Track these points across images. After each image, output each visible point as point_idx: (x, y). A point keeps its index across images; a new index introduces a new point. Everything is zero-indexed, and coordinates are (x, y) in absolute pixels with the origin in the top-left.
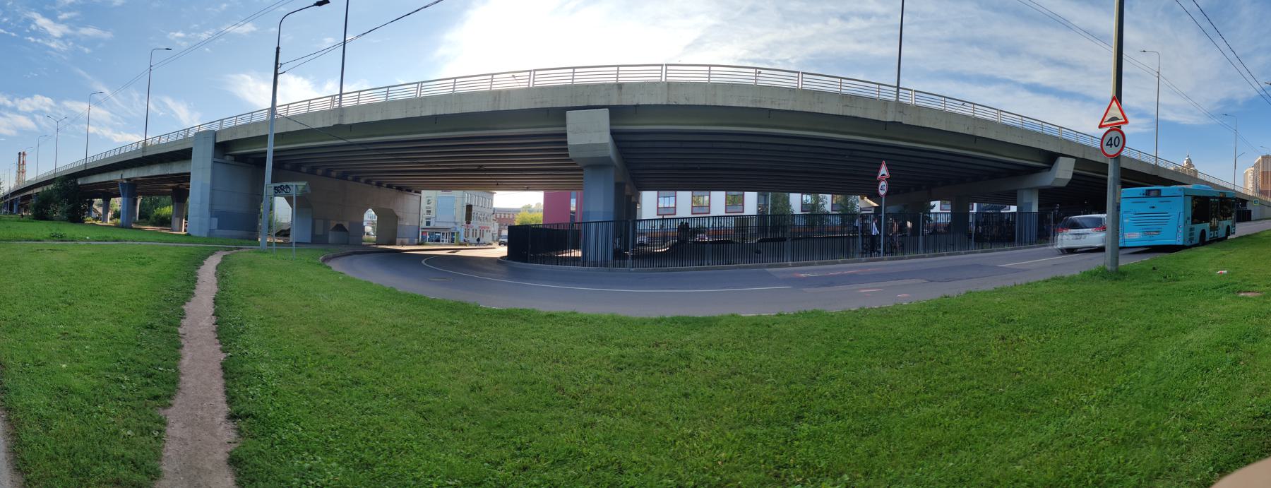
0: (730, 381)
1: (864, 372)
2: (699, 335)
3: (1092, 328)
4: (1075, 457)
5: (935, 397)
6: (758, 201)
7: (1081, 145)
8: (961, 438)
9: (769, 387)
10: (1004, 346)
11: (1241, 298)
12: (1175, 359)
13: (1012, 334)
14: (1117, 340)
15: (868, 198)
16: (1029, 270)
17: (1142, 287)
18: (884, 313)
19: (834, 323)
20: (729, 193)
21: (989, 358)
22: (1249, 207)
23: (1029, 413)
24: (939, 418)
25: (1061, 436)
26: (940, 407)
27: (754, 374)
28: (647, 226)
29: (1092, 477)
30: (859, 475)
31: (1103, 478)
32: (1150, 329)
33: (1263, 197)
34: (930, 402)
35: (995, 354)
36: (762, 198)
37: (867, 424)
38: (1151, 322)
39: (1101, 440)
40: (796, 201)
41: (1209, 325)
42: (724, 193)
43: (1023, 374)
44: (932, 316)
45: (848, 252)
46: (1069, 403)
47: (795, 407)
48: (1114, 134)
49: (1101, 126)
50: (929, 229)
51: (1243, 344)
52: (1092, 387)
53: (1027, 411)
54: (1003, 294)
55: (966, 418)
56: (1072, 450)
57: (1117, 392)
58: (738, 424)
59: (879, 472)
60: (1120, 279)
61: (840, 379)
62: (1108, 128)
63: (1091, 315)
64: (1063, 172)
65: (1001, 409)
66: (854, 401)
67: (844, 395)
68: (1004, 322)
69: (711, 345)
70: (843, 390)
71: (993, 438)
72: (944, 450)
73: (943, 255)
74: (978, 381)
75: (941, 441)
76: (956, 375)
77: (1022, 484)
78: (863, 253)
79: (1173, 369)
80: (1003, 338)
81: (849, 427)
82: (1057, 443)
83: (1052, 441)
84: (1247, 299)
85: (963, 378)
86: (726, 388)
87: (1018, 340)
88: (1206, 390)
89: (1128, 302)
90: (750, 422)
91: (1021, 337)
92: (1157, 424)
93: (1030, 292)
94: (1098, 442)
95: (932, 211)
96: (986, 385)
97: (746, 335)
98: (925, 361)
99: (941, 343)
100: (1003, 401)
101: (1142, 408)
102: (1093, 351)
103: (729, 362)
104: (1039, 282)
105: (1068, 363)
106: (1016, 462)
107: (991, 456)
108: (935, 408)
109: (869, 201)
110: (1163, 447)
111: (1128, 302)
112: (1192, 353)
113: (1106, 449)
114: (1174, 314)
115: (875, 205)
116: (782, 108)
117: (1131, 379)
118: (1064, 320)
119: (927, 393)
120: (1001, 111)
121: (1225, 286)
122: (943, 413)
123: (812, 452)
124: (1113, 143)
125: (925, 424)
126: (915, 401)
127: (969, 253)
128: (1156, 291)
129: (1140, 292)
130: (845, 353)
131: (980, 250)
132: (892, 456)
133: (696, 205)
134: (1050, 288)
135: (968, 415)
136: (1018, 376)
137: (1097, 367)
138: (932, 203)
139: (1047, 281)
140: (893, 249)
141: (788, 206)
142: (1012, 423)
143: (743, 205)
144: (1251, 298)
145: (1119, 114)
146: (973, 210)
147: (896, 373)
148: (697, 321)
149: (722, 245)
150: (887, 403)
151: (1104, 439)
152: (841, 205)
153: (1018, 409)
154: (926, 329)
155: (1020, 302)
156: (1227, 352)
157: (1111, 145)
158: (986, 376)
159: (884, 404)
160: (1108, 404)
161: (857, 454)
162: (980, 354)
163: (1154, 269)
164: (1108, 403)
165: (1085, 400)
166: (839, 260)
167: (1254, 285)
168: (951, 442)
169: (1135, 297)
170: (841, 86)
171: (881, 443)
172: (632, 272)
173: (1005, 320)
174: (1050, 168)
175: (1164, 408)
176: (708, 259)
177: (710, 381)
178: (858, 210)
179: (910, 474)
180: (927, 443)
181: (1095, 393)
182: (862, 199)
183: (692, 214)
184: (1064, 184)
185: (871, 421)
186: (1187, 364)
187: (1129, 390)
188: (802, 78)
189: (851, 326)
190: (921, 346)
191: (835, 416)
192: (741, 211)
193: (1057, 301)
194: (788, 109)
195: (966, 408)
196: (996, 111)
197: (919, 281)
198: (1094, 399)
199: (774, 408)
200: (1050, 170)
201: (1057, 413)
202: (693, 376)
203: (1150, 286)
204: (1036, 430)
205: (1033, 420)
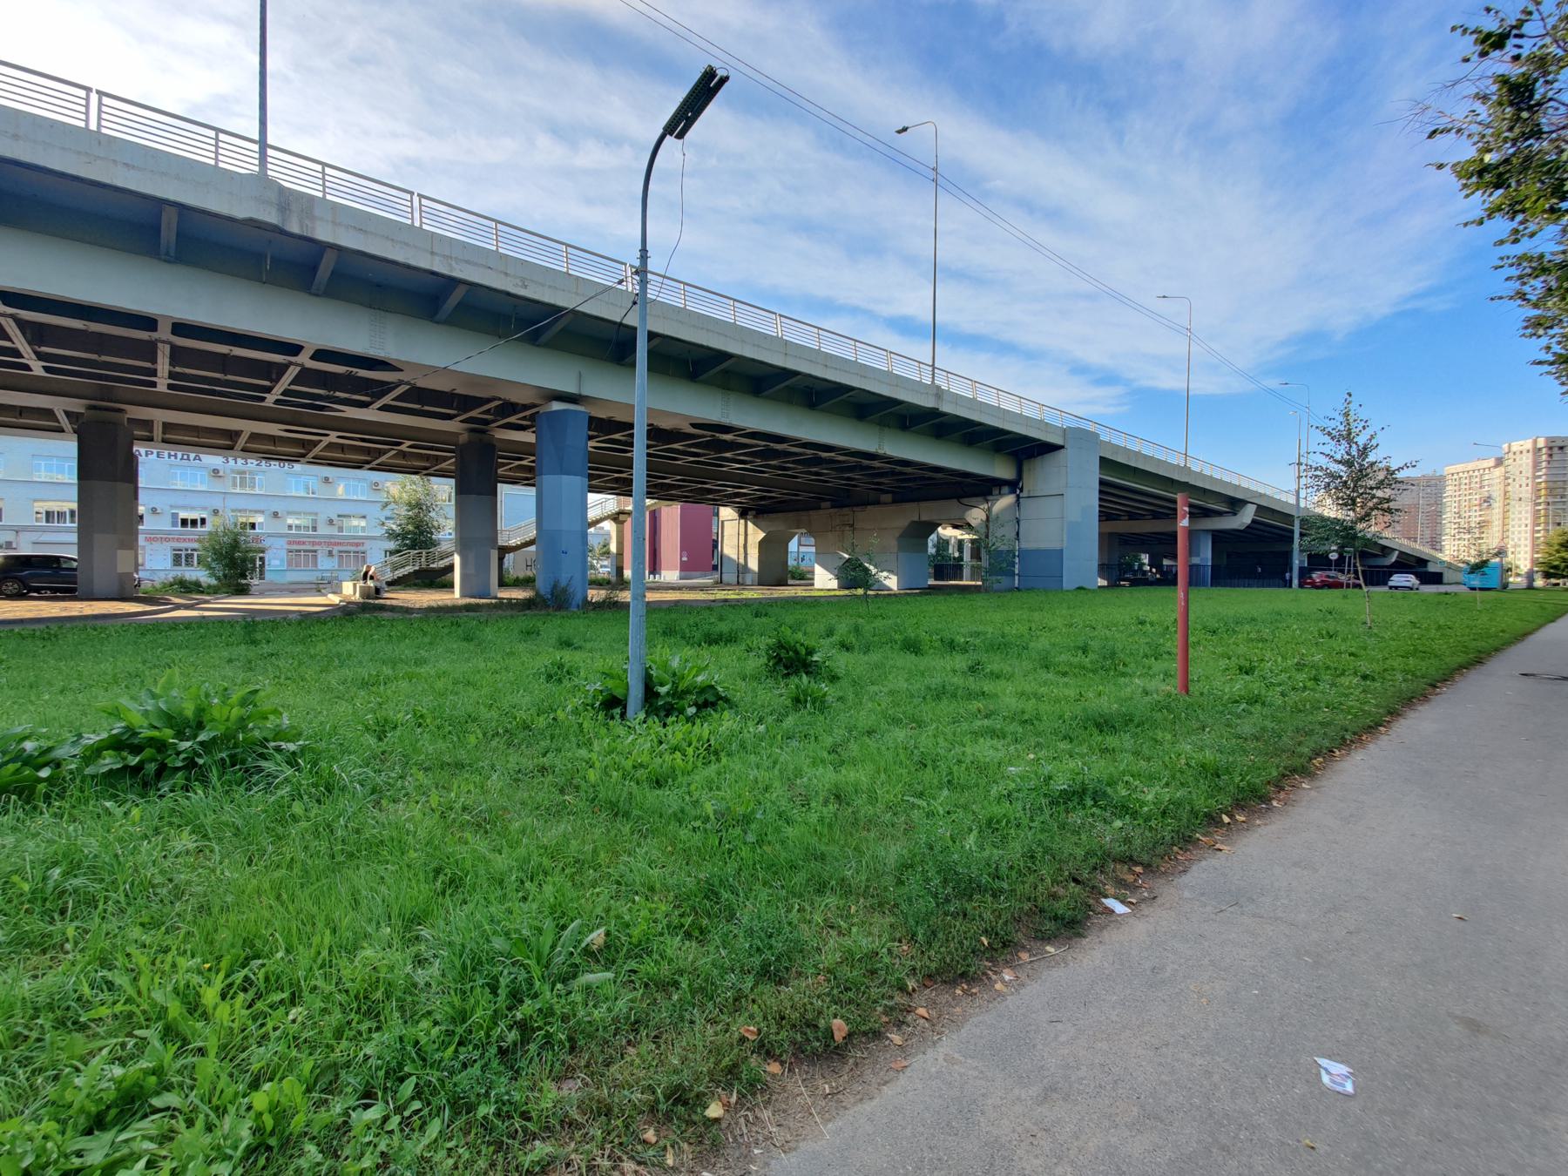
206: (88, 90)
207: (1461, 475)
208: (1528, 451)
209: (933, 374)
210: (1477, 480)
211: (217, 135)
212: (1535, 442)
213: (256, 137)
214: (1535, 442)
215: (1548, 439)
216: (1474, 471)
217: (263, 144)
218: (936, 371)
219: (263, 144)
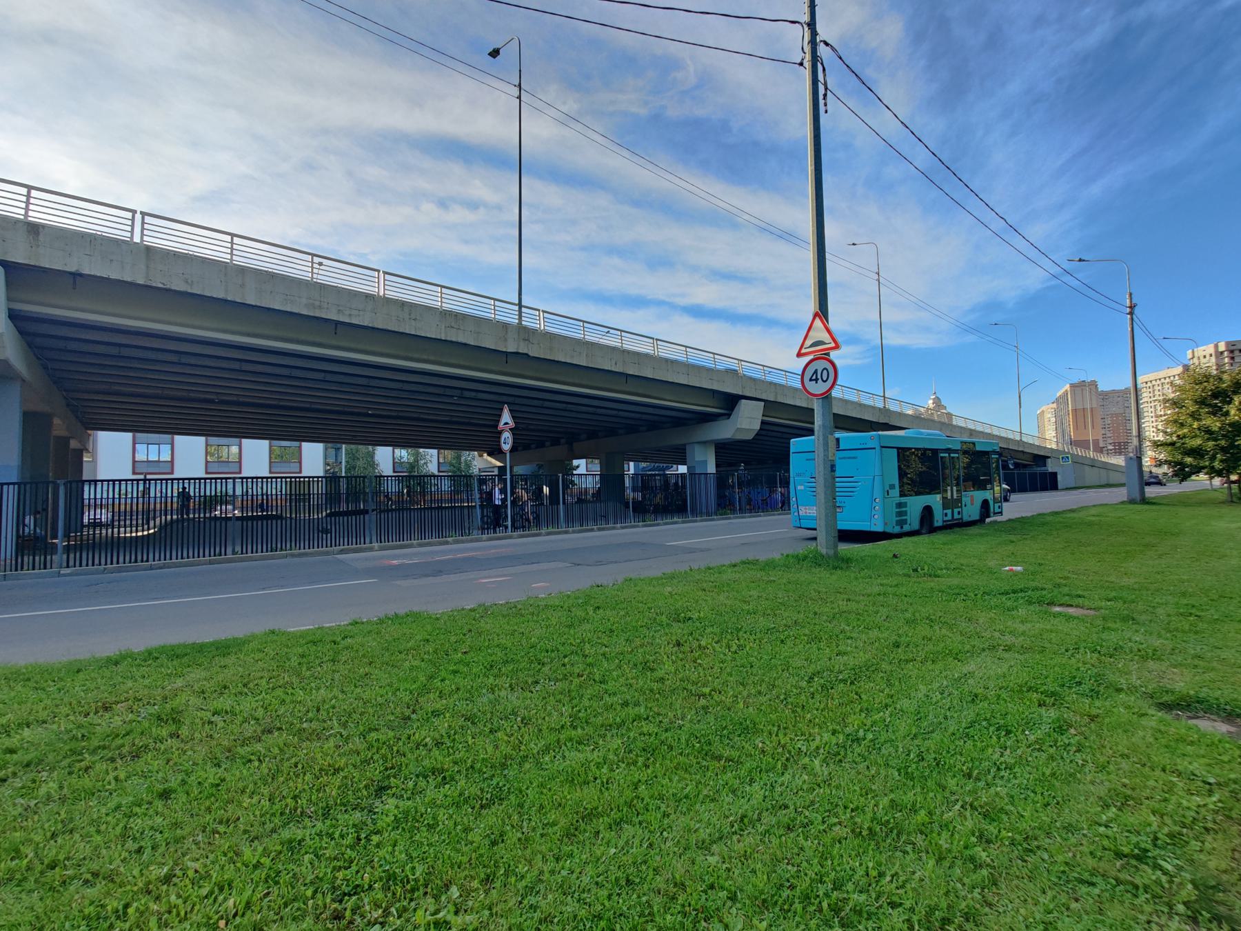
0: (259, 747)
1: (484, 700)
2: (204, 674)
3: (805, 635)
4: (796, 850)
5: (587, 734)
6: (326, 457)
7: (771, 383)
8: (626, 802)
9: (331, 743)
10: (681, 656)
11: (1055, 615)
12: (948, 704)
13: (690, 638)
14: (845, 658)
15: (489, 455)
16: (709, 550)
17: (879, 581)
18: (513, 611)
19: (440, 629)
20: (275, 443)
21: (660, 673)
22: (1051, 467)
23: (722, 762)
24: (593, 768)
25: (773, 807)
26: (593, 750)
27: (305, 725)
28: (101, 492)
29: (827, 895)
30: (475, 884)
31: (845, 900)
32: (898, 647)
33: (1079, 452)
34: (580, 743)
35: (669, 667)
36: (332, 452)
37: (489, 786)
38: (899, 636)
39: (835, 824)
40: (385, 458)
41: (1000, 653)
42: (266, 443)
43: (709, 698)
44: (579, 613)
45: (462, 527)
46: (780, 750)
47: (375, 772)
48: (820, 364)
49: (799, 355)
50: (571, 496)
51: (1071, 696)
52: (813, 728)
53: (719, 758)
54: (675, 581)
55: (632, 767)
56: (792, 835)
57: (853, 741)
58: (269, 826)
59: (506, 874)
60: (842, 569)
61: (447, 715)
62: (811, 357)
63: (802, 615)
64: (747, 421)
65: (681, 754)
66: (468, 748)
67: (454, 740)
68: (679, 621)
69: (225, 687)
70: (452, 732)
71: (672, 804)
72: (601, 824)
73: (592, 530)
74: (646, 707)
75: (596, 808)
76: (615, 699)
77: (721, 894)
78: (483, 529)
79: (946, 718)
80: (678, 644)
81: (460, 795)
82: (768, 819)
83: (760, 814)
84: (1069, 618)
85: (625, 704)
86: (250, 761)
87: (700, 646)
88: (1009, 768)
89: (858, 602)
90: (295, 816)
91: (703, 643)
92: (930, 813)
93: (712, 580)
94: (831, 827)
95: (575, 472)
96: (659, 714)
97: (294, 661)
98: (571, 678)
99: (593, 651)
100: (683, 741)
101: (898, 778)
102: (810, 670)
103: (260, 713)
104: (724, 566)
105: (774, 686)
106: (706, 849)
107: (671, 836)
108: (587, 754)
109: (489, 459)
110: (946, 863)
111: (858, 602)
112: (976, 696)
113: (844, 842)
114: (936, 628)
115: (499, 464)
116: (355, 321)
117: (874, 723)
118: (763, 622)
119: (575, 728)
120: (657, 340)
121: (1021, 591)
122: (599, 761)
123: (400, 853)
124: (819, 377)
125: (573, 779)
126: (558, 741)
127: (626, 527)
128: (903, 590)
129: (876, 589)
130: (455, 672)
131: (641, 524)
132: (525, 842)
133: (352, 457)
134: (740, 575)
135: (635, 763)
136: (703, 702)
137: (817, 697)
138: (575, 462)
139: (735, 566)
140: (522, 523)
141: (373, 465)
142: (698, 777)
143: (300, 463)
144: (1078, 618)
145: (825, 336)
146: (629, 470)
147: (531, 698)
148: (200, 648)
149: (260, 523)
150: (517, 748)
151: (840, 823)
152: (451, 465)
153: (706, 754)
154: (572, 632)
155: (700, 593)
156: (1040, 705)
157: (816, 380)
158: (658, 700)
159: (514, 749)
160: (840, 761)
161: (472, 843)
162: (647, 667)
163: (895, 556)
164: (839, 757)
165: (804, 749)
166: (450, 539)
167: (1080, 596)
168: (612, 810)
169: (869, 596)
170: (441, 297)
171: (509, 818)
172: (65, 575)
173: (679, 618)
174: (729, 416)
175: (940, 785)
176: (234, 545)
177: (218, 755)
178: (475, 471)
179: (552, 872)
180: (577, 813)
181: (818, 738)
182: (481, 456)
183: (207, 473)
184: (750, 436)
185: (494, 782)
186: (969, 714)
187: (872, 741)
188: (384, 280)
189: (464, 632)
190: (565, 657)
191: (439, 779)
192: (238, 471)
193: (751, 593)
194: (365, 324)
195: (630, 751)
196: (651, 341)
197: (561, 565)
198: (818, 748)
199: (337, 780)
200: (729, 418)
201: (763, 767)
202: (185, 752)
203: (892, 581)
204: (734, 792)
205: (729, 774)
206: (134, 212)
207: (1154, 382)
208: (1211, 355)
209: (28, 203)
210: (1160, 388)
211: (232, 239)
212: (1216, 346)
213: (517, 302)
214: (1216, 346)
215: (1228, 344)
216: (1165, 378)
217: (520, 305)
218: (524, 310)
219: (520, 305)
